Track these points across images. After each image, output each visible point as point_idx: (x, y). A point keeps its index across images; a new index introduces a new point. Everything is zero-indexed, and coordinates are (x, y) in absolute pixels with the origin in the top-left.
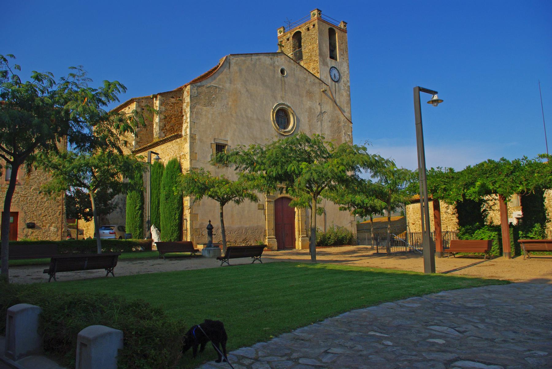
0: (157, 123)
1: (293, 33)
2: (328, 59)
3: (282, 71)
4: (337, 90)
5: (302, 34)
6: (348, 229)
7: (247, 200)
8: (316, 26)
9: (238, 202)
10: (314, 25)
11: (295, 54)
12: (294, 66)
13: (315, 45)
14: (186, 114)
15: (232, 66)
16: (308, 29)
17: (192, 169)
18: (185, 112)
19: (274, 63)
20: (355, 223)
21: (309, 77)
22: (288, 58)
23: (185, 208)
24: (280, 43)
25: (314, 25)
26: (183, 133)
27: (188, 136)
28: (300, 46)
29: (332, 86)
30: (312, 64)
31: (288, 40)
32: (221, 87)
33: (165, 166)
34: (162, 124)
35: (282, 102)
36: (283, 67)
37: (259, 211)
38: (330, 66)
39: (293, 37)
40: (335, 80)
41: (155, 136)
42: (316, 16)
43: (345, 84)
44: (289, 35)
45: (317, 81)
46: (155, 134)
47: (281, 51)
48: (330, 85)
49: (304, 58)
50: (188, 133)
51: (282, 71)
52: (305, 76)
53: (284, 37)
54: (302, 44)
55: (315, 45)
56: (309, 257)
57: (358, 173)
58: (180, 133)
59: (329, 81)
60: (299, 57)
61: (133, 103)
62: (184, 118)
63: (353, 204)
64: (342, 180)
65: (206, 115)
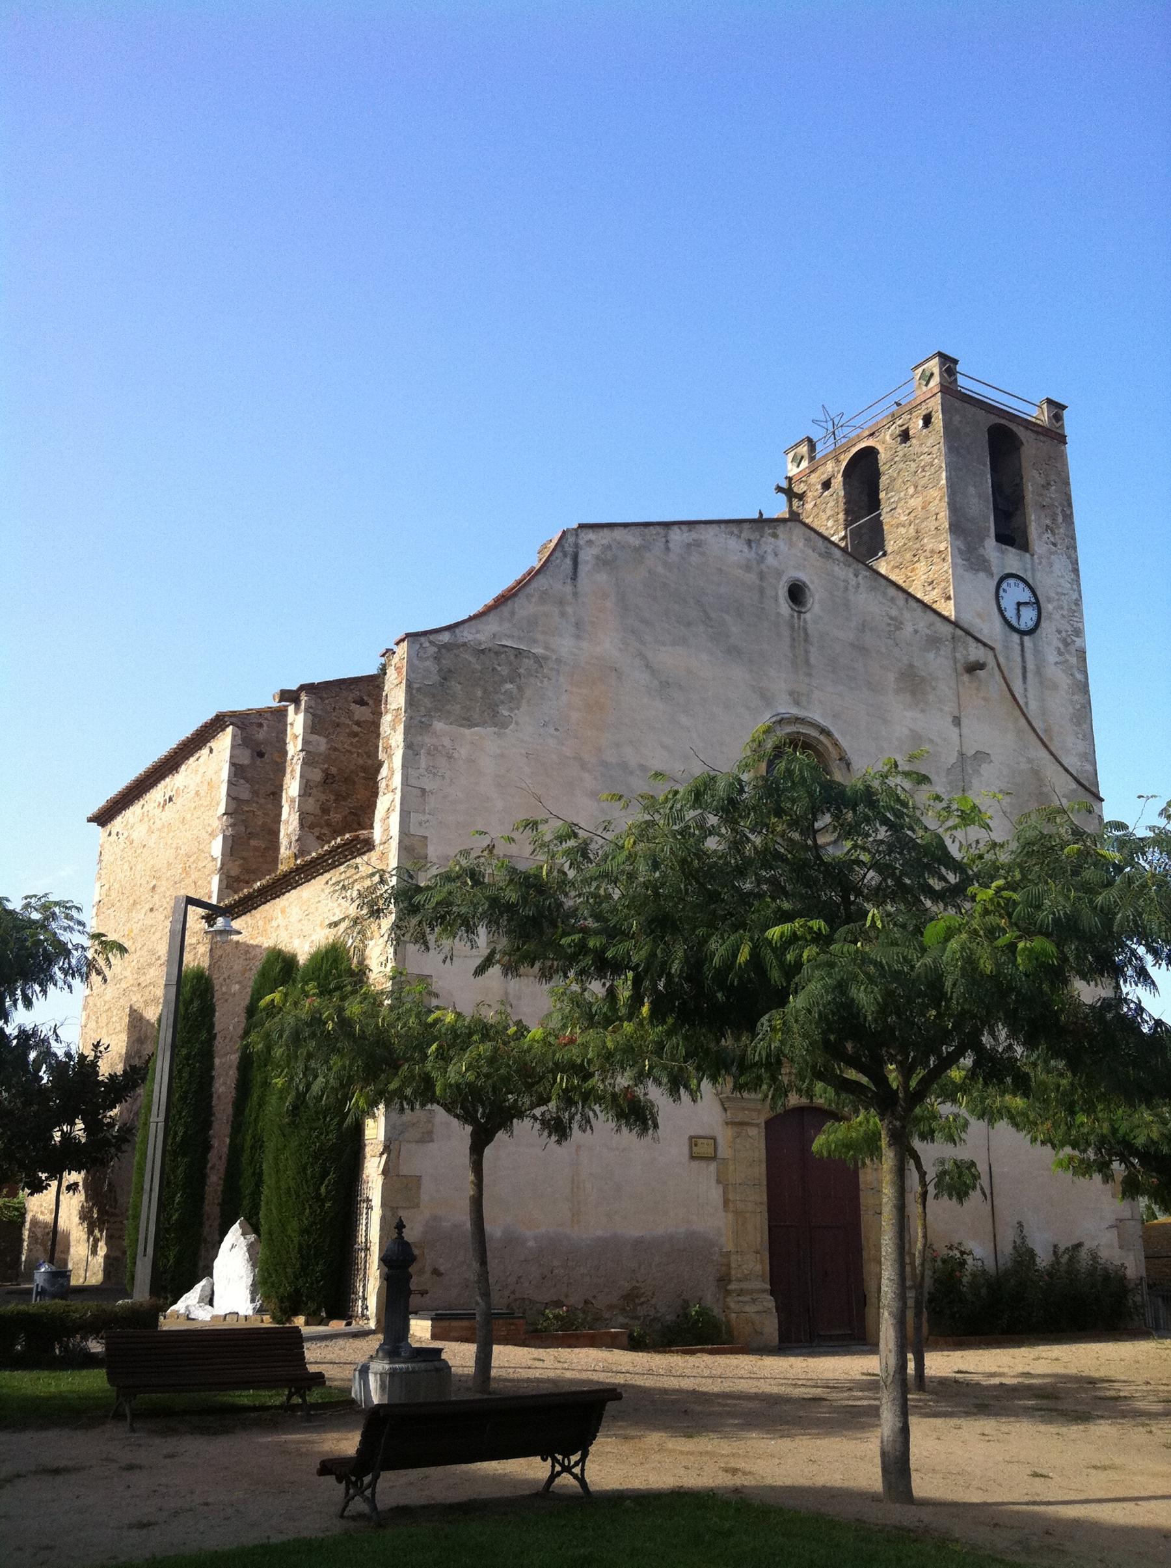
0: (293, 801)
1: (845, 459)
2: (991, 543)
3: (797, 593)
4: (1031, 666)
5: (883, 457)
6: (1104, 1254)
7: (603, 1121)
8: (938, 419)
9: (558, 1129)
10: (927, 420)
11: (856, 535)
12: (843, 572)
13: (934, 493)
14: (390, 756)
15: (583, 569)
16: (905, 436)
17: (398, 976)
18: (387, 748)
19: (762, 559)
20: (1135, 1229)
21: (907, 615)
22: (820, 543)
23: (369, 1150)
24: (785, 485)
25: (927, 420)
26: (377, 834)
27: (394, 844)
28: (874, 504)
29: (1006, 647)
30: (922, 567)
31: (826, 485)
32: (538, 650)
33: (301, 962)
34: (311, 805)
35: (794, 711)
36: (803, 576)
37: (695, 1164)
38: (998, 573)
39: (848, 473)
40: (1023, 627)
41: (284, 852)
42: (935, 381)
43: (1066, 644)
44: (830, 466)
45: (947, 629)
46: (284, 841)
47: (791, 512)
48: (998, 646)
49: (890, 546)
50: (395, 831)
51: (797, 593)
52: (894, 612)
53: (814, 478)
54: (882, 495)
55: (934, 493)
56: (909, 1396)
57: (1133, 991)
58: (363, 833)
59: (992, 629)
60: (867, 540)
61: (223, 730)
62: (384, 772)
63: (1124, 1148)
64: (1043, 1020)
65: (471, 761)
